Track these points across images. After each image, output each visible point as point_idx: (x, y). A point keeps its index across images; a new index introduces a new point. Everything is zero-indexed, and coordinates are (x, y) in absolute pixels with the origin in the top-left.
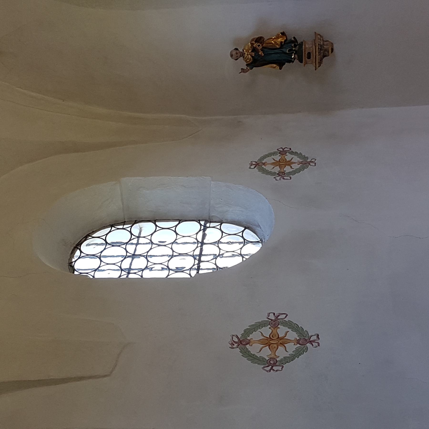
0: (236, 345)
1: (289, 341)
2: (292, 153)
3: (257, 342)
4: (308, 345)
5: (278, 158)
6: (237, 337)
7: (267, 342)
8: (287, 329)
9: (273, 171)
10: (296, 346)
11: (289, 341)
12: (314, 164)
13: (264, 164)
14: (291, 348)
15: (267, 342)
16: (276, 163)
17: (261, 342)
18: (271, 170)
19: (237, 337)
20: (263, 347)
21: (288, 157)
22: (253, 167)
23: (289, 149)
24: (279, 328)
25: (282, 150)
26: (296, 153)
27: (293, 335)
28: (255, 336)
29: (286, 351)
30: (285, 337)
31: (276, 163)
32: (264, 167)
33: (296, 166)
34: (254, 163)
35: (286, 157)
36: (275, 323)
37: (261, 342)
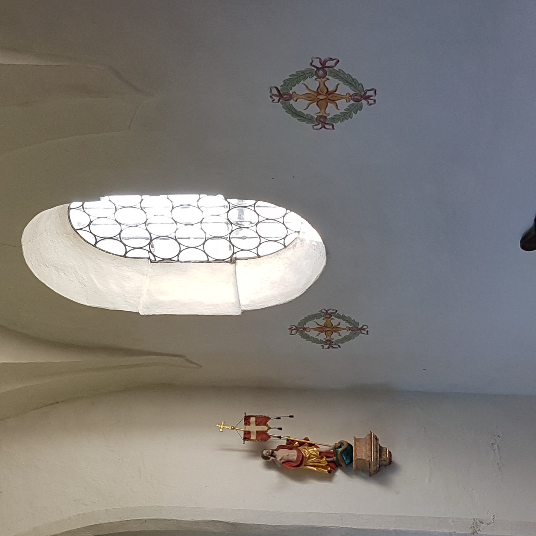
0: (277, 99)
1: (341, 97)
2: (339, 317)
3: (303, 97)
4: (364, 102)
5: (322, 322)
6: (277, 88)
7: (331, 96)
8: (337, 81)
9: (319, 338)
10: (349, 103)
11: (341, 97)
12: (365, 332)
13: (305, 329)
14: (343, 105)
15: (331, 96)
16: (321, 329)
17: (307, 97)
18: (317, 337)
19: (277, 88)
20: (309, 104)
21: (335, 321)
22: (294, 332)
23: (334, 311)
24: (328, 79)
25: (325, 312)
26: (343, 318)
27: (344, 89)
28: (299, 89)
29: (337, 108)
30: (335, 91)
31: (321, 329)
32: (308, 333)
33: (345, 333)
34: (294, 328)
35: (332, 321)
36: (323, 69)
37: (307, 97)
